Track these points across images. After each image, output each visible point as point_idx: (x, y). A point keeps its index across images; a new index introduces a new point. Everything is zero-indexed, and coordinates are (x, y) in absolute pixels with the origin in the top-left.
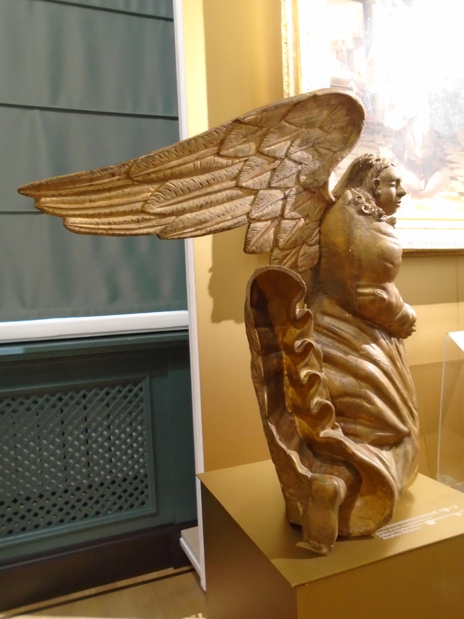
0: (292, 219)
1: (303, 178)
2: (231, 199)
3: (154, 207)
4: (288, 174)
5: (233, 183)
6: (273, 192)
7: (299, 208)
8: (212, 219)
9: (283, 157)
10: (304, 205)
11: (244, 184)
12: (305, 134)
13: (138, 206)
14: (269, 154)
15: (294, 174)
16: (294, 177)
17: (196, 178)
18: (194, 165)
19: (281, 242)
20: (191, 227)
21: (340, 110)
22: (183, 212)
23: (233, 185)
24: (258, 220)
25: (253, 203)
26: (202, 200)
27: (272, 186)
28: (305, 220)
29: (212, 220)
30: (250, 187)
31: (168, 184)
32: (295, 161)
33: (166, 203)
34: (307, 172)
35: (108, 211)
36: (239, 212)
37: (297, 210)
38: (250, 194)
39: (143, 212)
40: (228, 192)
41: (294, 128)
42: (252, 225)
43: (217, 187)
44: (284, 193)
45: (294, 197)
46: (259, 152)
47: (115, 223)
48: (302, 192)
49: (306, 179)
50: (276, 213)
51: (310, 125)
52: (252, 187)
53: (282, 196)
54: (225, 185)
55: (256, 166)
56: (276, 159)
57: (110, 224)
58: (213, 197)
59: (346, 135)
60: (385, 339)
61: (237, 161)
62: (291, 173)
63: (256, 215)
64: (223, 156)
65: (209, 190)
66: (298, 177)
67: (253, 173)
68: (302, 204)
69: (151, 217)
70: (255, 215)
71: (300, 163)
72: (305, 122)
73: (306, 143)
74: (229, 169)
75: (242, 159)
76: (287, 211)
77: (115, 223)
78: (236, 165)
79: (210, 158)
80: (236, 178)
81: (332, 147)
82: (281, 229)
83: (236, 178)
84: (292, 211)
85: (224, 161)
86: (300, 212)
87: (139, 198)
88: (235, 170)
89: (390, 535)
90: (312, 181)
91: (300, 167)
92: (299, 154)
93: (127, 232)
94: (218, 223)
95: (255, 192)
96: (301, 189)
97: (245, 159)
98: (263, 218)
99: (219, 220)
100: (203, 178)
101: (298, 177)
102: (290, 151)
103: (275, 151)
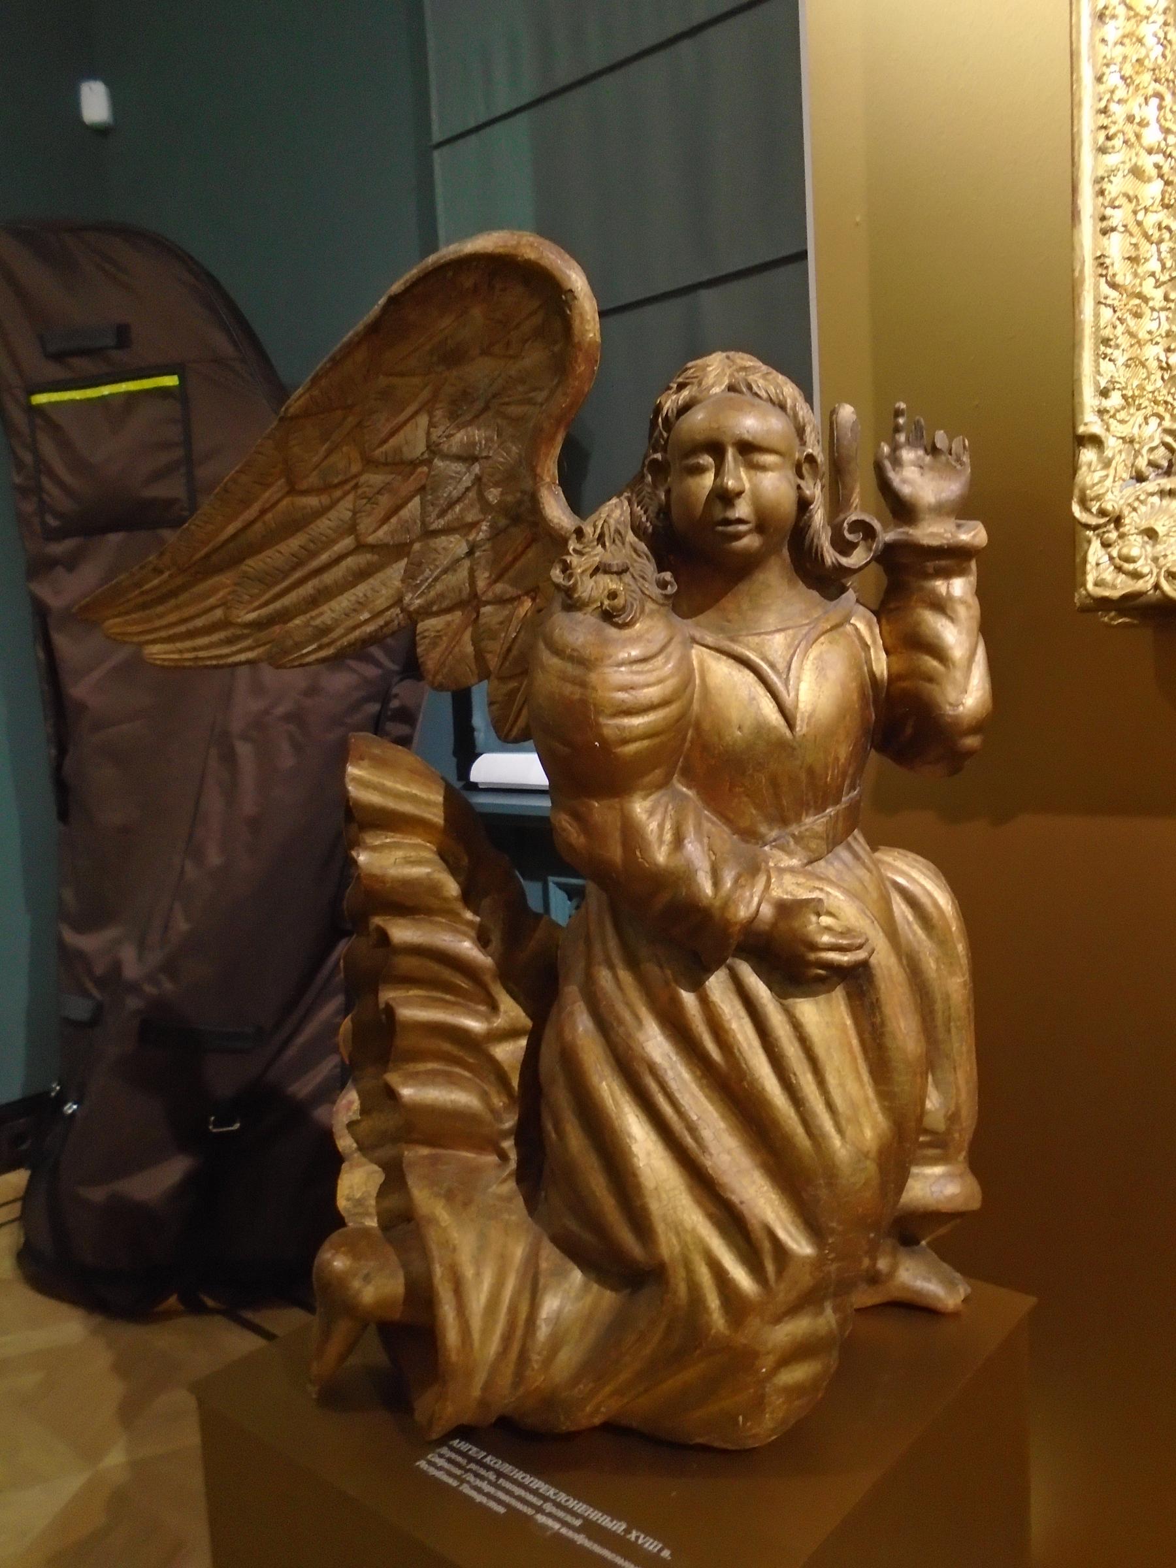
0: (501, 601)
1: (493, 495)
2: (362, 575)
3: (242, 613)
4: (455, 494)
5: (348, 542)
6: (442, 541)
7: (511, 573)
8: (337, 623)
9: (426, 456)
10: (523, 560)
11: (371, 539)
12: (453, 385)
13: (218, 613)
14: (389, 460)
15: (468, 489)
16: (472, 494)
17: (282, 547)
18: (264, 523)
19: (493, 662)
20: (310, 642)
21: (504, 290)
22: (284, 616)
23: (352, 547)
24: (426, 612)
25: (409, 576)
26: (308, 588)
27: (434, 527)
28: (534, 599)
29: (338, 626)
30: (385, 541)
31: (243, 567)
32: (458, 458)
33: (256, 604)
34: (498, 477)
35: (182, 628)
36: (380, 603)
37: (506, 577)
38: (398, 558)
39: (225, 624)
40: (350, 561)
41: (416, 380)
42: (421, 627)
43: (324, 557)
44: (467, 541)
45: (487, 546)
46: (370, 463)
47: (201, 648)
48: (507, 527)
49: (502, 494)
50: (460, 591)
51: (453, 357)
52: (388, 540)
53: (463, 548)
54: (338, 548)
55: (378, 493)
56: (414, 464)
57: (195, 649)
58: (328, 578)
59: (556, 348)
60: (661, 967)
61: (338, 493)
62: (461, 488)
63: (418, 601)
64: (304, 493)
65: (315, 564)
66: (481, 497)
67: (380, 512)
68: (515, 560)
69: (245, 631)
70: (415, 602)
71: (474, 459)
72: (435, 359)
73: (463, 406)
74: (333, 514)
75: (347, 487)
76: (481, 584)
77: (201, 648)
78: (342, 503)
79: (284, 502)
80: (352, 528)
81: (531, 395)
82: (482, 630)
83: (352, 528)
84: (496, 581)
85: (313, 501)
86: (514, 583)
87: (212, 601)
88: (343, 511)
89: (539, 1510)
90: (519, 495)
91: (476, 468)
92: (461, 436)
93: (221, 662)
94: (354, 628)
95: (399, 550)
96: (503, 522)
97: (352, 483)
98: (435, 608)
99: (350, 623)
100: (294, 543)
101: (481, 497)
102: (434, 438)
103: (398, 450)
